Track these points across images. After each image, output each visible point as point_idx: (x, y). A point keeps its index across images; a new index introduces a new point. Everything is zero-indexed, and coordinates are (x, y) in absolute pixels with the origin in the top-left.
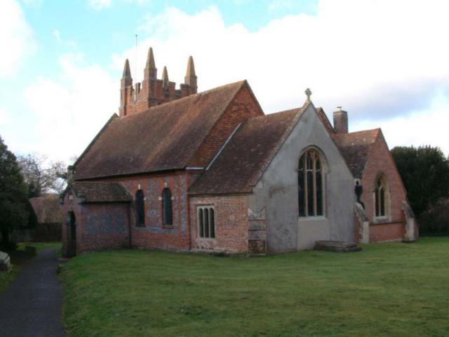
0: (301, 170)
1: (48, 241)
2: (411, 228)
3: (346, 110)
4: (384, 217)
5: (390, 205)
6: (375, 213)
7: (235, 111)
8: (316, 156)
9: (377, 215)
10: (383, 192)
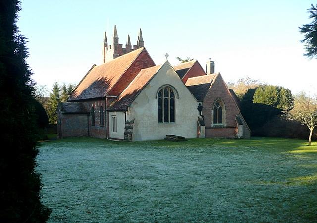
0: (160, 98)
1: (194, 76)
2: (239, 131)
3: (213, 61)
4: (221, 124)
5: (225, 117)
6: (213, 122)
7: (138, 65)
8: (171, 91)
9: (215, 122)
10: (221, 109)
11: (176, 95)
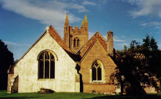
0: (52, 60)
4: (100, 81)
10: (100, 70)
11: (55, 58)
